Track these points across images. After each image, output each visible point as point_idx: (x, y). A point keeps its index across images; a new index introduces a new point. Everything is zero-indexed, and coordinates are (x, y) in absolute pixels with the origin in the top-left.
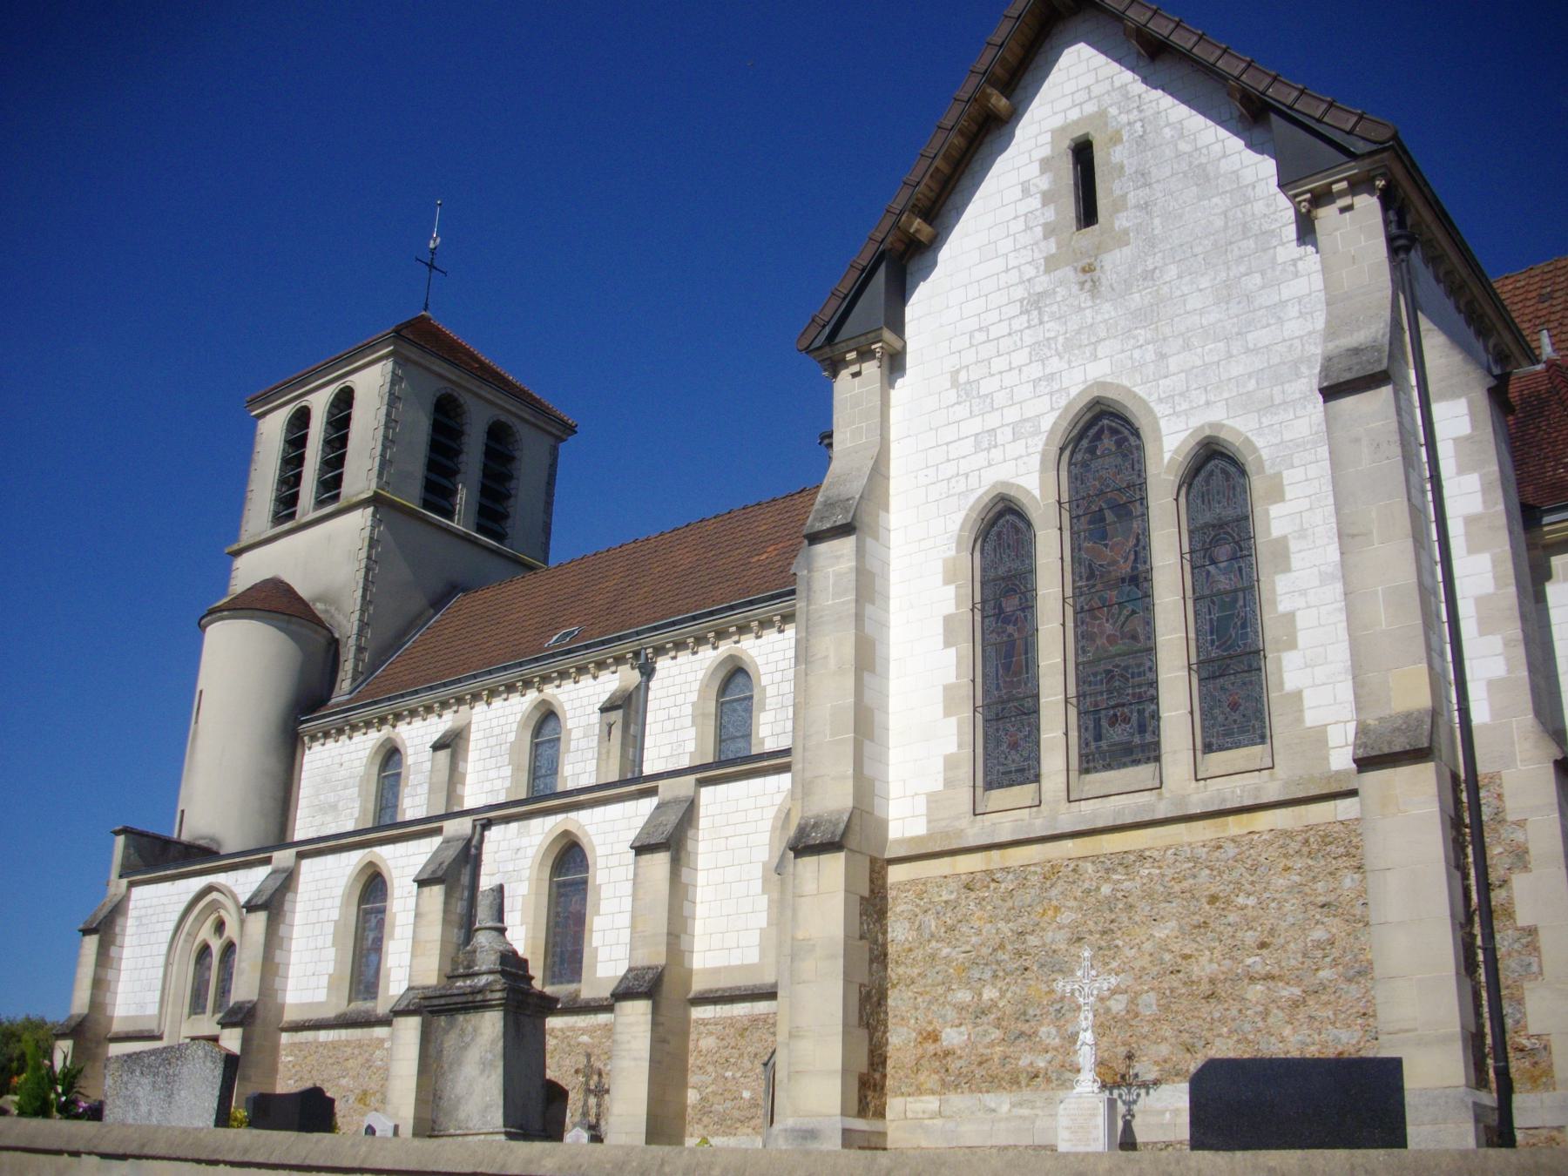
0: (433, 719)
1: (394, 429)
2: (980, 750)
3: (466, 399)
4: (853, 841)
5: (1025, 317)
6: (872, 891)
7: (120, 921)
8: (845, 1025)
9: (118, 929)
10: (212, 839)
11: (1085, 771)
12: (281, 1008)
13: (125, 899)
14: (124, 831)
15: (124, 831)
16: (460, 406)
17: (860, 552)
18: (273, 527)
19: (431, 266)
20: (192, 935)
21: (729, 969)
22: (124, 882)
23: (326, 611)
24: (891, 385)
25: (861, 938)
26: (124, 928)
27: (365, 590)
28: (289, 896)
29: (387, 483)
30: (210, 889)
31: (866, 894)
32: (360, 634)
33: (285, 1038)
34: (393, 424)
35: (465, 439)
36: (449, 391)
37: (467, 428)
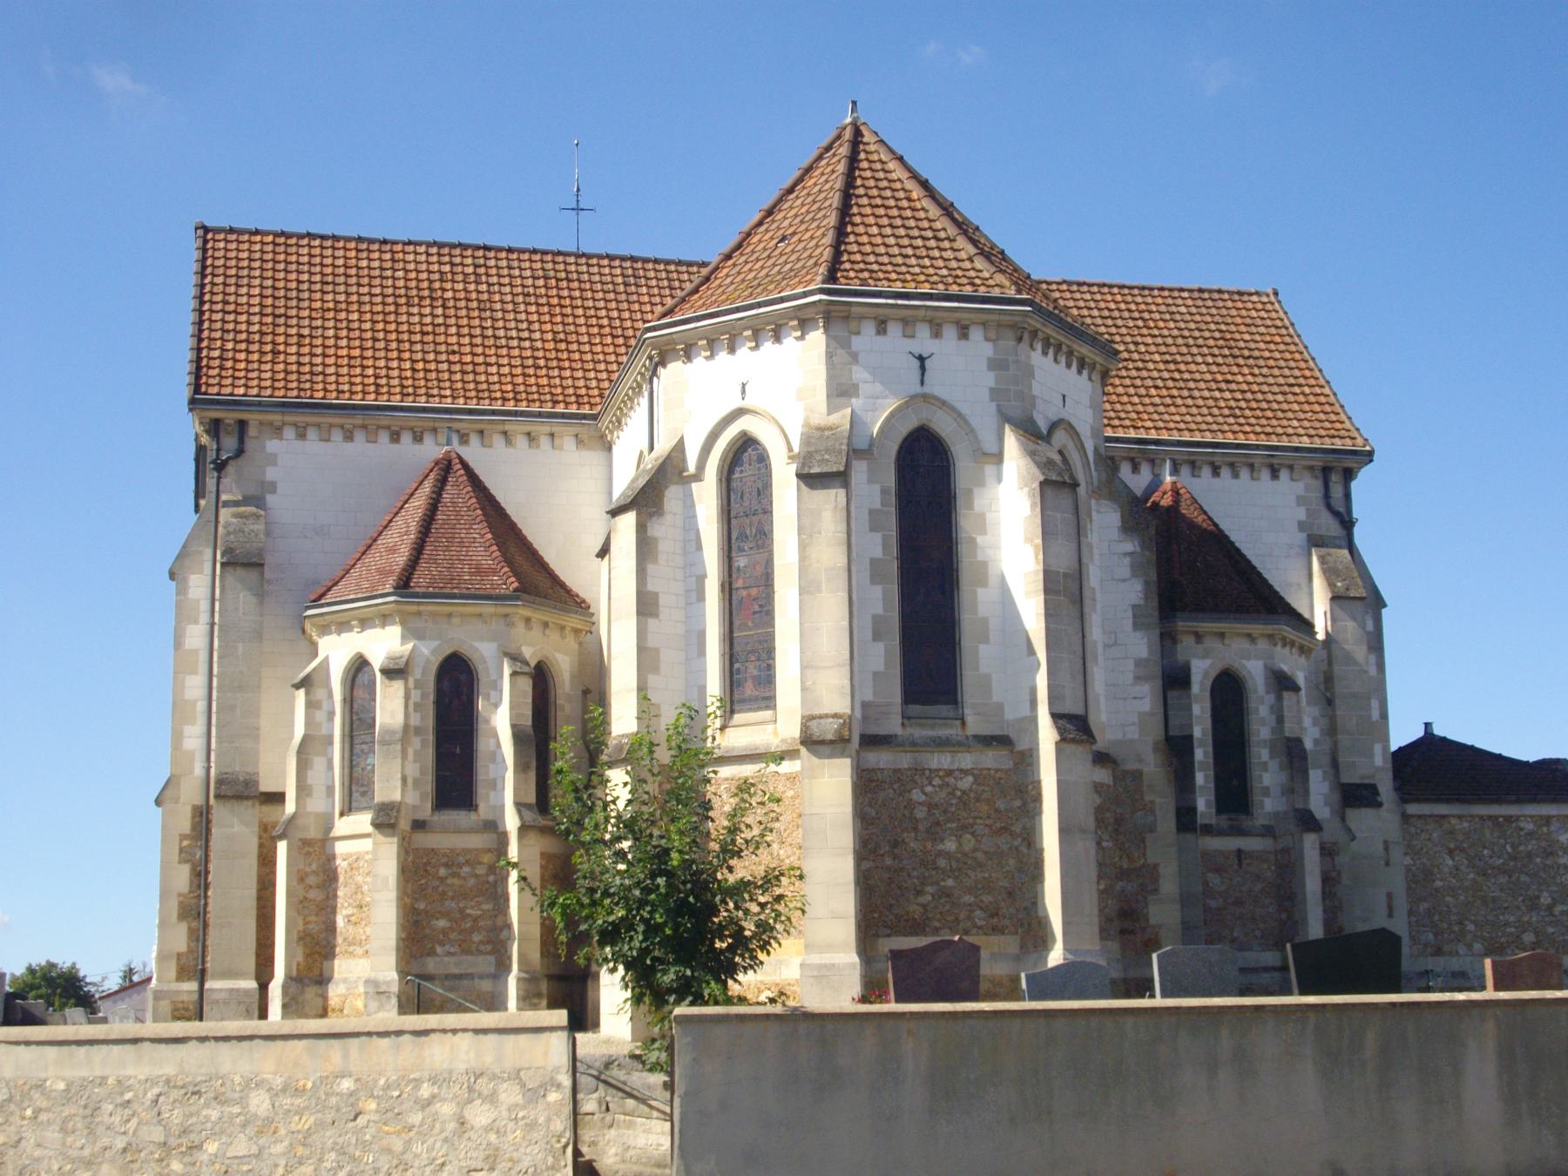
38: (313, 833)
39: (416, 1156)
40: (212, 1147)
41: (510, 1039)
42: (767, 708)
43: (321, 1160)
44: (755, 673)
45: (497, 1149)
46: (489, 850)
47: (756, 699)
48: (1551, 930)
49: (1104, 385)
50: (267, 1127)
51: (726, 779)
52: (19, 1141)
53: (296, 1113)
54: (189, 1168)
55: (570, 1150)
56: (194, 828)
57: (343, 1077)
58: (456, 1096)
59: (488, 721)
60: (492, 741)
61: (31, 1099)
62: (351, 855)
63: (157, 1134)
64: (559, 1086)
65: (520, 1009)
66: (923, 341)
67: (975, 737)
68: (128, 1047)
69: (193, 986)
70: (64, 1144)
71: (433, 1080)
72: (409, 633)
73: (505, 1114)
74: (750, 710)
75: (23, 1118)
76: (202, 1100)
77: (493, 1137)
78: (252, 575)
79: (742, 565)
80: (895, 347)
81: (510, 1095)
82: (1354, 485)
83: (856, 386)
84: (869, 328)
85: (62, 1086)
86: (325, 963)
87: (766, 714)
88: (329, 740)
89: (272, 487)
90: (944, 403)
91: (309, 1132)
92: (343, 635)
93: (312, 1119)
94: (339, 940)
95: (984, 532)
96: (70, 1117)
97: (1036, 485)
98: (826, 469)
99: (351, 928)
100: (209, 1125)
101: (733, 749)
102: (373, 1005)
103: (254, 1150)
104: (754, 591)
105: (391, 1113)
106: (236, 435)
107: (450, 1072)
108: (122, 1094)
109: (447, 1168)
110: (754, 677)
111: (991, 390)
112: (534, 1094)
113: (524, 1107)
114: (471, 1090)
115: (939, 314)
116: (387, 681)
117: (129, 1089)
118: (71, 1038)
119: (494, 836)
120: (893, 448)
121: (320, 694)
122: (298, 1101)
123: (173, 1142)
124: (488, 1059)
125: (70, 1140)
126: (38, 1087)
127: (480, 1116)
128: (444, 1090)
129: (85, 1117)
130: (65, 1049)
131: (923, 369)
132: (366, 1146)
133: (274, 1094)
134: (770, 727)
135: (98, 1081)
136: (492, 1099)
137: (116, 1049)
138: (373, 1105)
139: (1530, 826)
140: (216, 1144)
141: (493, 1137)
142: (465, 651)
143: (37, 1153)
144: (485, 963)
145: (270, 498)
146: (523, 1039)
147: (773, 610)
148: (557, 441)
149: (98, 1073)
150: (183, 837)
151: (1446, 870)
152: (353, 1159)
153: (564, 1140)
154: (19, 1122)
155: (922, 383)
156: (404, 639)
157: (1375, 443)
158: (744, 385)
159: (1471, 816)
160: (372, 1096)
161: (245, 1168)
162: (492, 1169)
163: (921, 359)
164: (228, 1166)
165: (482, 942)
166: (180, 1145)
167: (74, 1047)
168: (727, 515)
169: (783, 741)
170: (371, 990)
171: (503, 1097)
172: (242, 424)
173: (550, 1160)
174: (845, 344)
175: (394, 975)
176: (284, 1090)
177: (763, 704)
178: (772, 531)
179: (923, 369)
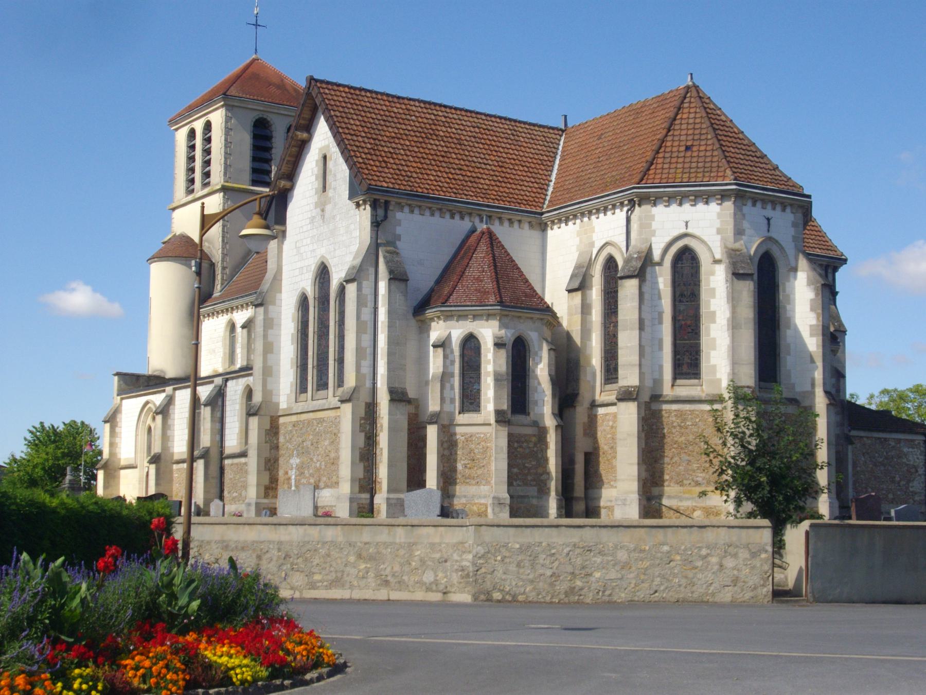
0: (245, 311)
1: (230, 147)
2: (298, 381)
3: (271, 118)
4: (262, 412)
5: (309, 226)
6: (271, 427)
7: (119, 416)
8: (258, 470)
9: (118, 420)
10: (162, 371)
11: (318, 390)
12: (173, 454)
13: (120, 405)
14: (118, 374)
15: (118, 374)
16: (268, 122)
17: (266, 312)
18: (186, 196)
19: (256, 25)
20: (144, 422)
21: (508, 399)
22: (119, 398)
23: (209, 247)
24: (283, 243)
25: (266, 442)
26: (121, 419)
27: (223, 237)
28: (171, 407)
29: (230, 178)
30: (147, 403)
31: (268, 427)
32: (223, 260)
33: (175, 467)
34: (229, 145)
35: (273, 140)
36: (261, 116)
37: (274, 134)
38: (446, 422)
39: (699, 579)
40: (597, 575)
41: (744, 531)
42: (695, 378)
43: (653, 581)
44: (689, 361)
45: (737, 577)
46: (534, 435)
47: (689, 374)
48: (899, 493)
49: (805, 229)
50: (626, 566)
51: (675, 410)
52: (493, 571)
53: (641, 560)
54: (585, 584)
55: (771, 578)
56: (366, 413)
57: (664, 545)
58: (718, 554)
59: (534, 371)
60: (536, 382)
61: (500, 552)
62: (467, 434)
63: (569, 569)
64: (766, 551)
65: (559, 516)
66: (769, 212)
67: (786, 399)
68: (553, 529)
69: (367, 496)
70: (518, 573)
71: (708, 547)
72: (503, 326)
73: (741, 562)
74: (686, 379)
75: (496, 561)
76: (592, 554)
77: (735, 572)
78: (402, 285)
79: (682, 309)
80: (755, 213)
81: (744, 554)
82: (837, 274)
83: (744, 230)
84: (750, 203)
85: (518, 546)
86: (450, 487)
87: (695, 381)
88: (452, 375)
89: (398, 238)
90: (777, 241)
91: (646, 569)
92: (460, 322)
93: (648, 564)
94: (459, 476)
95: (789, 304)
96: (521, 561)
97: (819, 285)
98: (746, 272)
99: (467, 470)
100: (596, 565)
101: (680, 397)
102: (497, 509)
103: (620, 576)
104: (689, 322)
105: (687, 561)
106: (383, 208)
107: (716, 544)
108: (550, 550)
109: (714, 585)
110: (688, 363)
111: (793, 236)
112: (754, 555)
113: (750, 560)
114: (726, 552)
115: (757, 196)
116: (497, 349)
117: (554, 548)
118: (523, 524)
119: (537, 429)
120: (756, 260)
121: (448, 351)
122: (641, 555)
123: (577, 572)
124: (734, 539)
125: (522, 571)
126: (504, 546)
127: (729, 563)
128: (713, 551)
129: (530, 561)
130: (520, 529)
131: (769, 224)
132: (675, 576)
133: (629, 552)
134: (699, 388)
135: (537, 544)
136: (735, 556)
137: (547, 530)
138: (678, 558)
139: (893, 444)
140: (599, 574)
141: (735, 572)
142: (475, 332)
143: (504, 577)
144: (533, 491)
145: (398, 243)
146: (751, 531)
147: (700, 331)
148: (522, 225)
149: (537, 540)
150: (362, 419)
151: (862, 462)
152: (668, 580)
153: (768, 574)
154: (493, 562)
155: (768, 231)
156: (500, 328)
157: (847, 254)
158: (687, 223)
159: (872, 437)
160: (678, 554)
161: (615, 584)
162: (735, 586)
163: (768, 220)
164: (606, 583)
165: (531, 480)
166: (581, 574)
167: (524, 529)
168: (675, 284)
169: (707, 395)
170: (496, 502)
171: (740, 555)
172: (387, 203)
173: (762, 582)
174: (741, 210)
175: (507, 496)
176: (634, 550)
177: (693, 376)
178: (699, 294)
179: (769, 224)
